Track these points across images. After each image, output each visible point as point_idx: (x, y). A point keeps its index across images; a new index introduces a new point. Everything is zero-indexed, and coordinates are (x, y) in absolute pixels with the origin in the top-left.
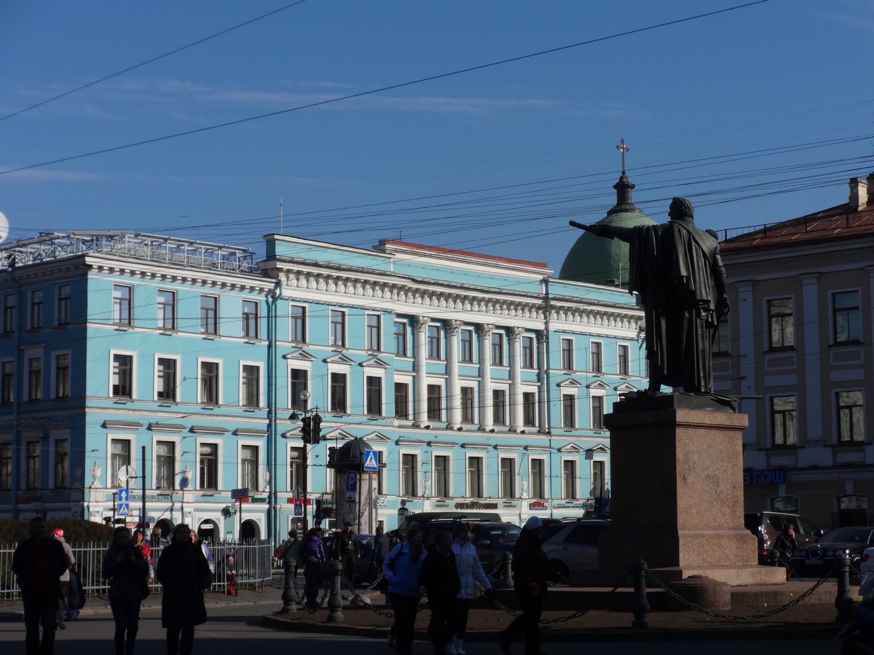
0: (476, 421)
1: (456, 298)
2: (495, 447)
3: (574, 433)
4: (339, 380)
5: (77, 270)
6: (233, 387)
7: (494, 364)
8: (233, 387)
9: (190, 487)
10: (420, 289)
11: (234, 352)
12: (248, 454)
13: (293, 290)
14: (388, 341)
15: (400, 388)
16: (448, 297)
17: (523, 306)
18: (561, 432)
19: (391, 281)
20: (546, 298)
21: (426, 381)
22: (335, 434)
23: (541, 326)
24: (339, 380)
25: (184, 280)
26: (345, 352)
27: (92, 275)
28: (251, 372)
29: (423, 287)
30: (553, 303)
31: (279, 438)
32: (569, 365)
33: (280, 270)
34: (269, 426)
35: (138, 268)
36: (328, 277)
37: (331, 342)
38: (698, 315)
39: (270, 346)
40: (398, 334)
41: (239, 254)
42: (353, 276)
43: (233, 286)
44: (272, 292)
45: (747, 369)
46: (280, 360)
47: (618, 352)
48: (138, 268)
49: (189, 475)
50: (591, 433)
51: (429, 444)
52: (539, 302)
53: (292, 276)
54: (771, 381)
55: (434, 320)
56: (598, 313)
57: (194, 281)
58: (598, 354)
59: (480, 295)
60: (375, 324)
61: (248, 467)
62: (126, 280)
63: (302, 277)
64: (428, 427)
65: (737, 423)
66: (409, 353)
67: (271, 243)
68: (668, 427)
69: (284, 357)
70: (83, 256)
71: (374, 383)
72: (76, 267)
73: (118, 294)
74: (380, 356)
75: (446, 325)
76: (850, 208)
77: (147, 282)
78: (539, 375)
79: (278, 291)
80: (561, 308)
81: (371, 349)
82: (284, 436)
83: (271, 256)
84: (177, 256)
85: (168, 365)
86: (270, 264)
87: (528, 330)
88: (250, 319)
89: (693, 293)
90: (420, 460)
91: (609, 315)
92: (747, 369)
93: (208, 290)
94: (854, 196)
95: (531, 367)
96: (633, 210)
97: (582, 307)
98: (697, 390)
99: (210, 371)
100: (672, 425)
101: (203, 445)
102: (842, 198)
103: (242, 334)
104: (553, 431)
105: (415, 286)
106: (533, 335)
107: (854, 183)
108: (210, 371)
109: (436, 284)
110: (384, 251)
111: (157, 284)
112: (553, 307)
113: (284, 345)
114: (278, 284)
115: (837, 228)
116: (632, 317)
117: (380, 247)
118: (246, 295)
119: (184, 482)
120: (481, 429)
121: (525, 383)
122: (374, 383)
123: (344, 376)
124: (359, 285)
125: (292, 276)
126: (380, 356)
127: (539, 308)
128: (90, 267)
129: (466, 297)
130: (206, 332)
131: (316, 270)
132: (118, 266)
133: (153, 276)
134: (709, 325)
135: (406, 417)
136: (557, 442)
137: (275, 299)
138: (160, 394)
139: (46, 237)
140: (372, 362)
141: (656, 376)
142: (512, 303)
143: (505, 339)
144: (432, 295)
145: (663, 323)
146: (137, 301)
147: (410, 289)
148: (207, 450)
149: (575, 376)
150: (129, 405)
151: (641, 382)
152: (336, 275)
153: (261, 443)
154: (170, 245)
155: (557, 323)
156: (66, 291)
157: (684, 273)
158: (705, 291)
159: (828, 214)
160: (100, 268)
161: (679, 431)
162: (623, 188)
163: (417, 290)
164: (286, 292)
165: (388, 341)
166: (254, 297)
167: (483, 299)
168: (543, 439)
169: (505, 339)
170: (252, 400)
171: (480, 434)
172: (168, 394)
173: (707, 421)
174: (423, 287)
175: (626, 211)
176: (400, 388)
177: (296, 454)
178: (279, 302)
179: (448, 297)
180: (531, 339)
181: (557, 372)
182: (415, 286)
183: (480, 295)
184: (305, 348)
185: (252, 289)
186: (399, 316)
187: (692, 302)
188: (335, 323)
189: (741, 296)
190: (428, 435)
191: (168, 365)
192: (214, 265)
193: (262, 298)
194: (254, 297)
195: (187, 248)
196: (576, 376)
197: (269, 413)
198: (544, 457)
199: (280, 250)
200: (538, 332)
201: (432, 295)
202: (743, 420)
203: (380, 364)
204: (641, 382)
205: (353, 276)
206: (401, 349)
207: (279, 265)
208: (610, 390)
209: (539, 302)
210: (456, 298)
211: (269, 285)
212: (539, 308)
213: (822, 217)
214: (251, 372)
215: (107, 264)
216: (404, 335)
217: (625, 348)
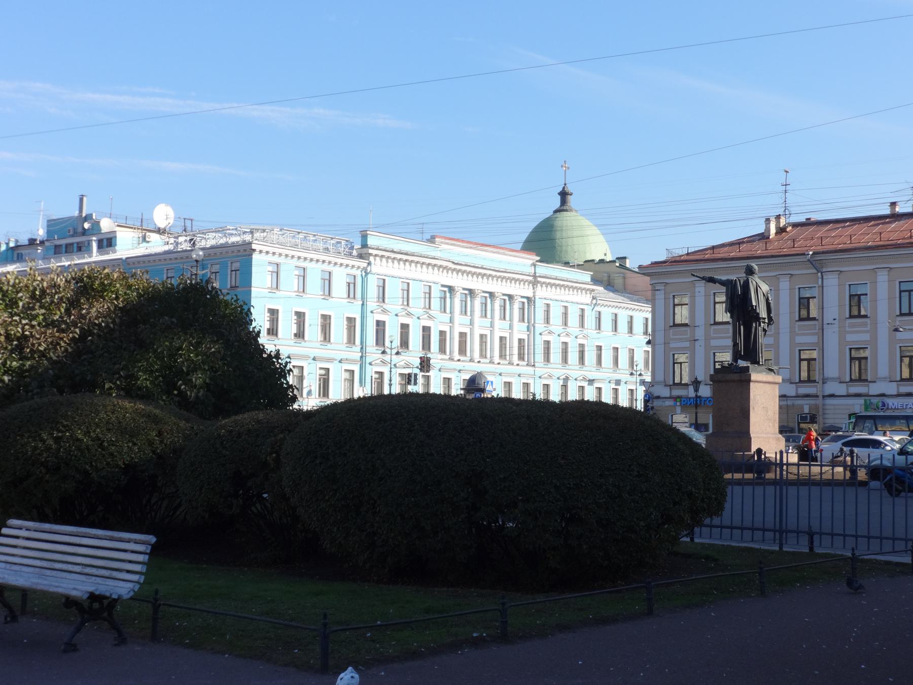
0: (488, 356)
1: (478, 275)
2: (500, 374)
3: (549, 366)
4: (405, 328)
5: (245, 252)
6: (338, 330)
7: (500, 319)
8: (338, 330)
9: (313, 396)
10: (457, 268)
11: (341, 309)
12: (347, 375)
13: (379, 267)
14: (436, 303)
15: (442, 333)
16: (473, 274)
17: (520, 281)
18: (542, 365)
19: (439, 263)
20: (535, 276)
21: (458, 330)
22: (402, 363)
23: (530, 295)
24: (405, 328)
25: (311, 260)
26: (409, 309)
27: (255, 256)
28: (351, 321)
29: (458, 267)
30: (539, 279)
31: (367, 365)
32: (547, 320)
33: (371, 254)
34: (362, 357)
35: (284, 252)
36: (382, 256)
37: (423, 306)
38: (760, 325)
39: (363, 304)
40: (379, 286)
41: (343, 243)
42: (416, 259)
43: (341, 265)
44: (365, 269)
45: (700, 333)
46: (369, 314)
47: (579, 313)
48: (284, 252)
49: (313, 388)
50: (560, 366)
51: (459, 371)
52: (531, 278)
53: (378, 258)
54: (714, 343)
55: (464, 289)
56: (567, 286)
57: (318, 261)
58: (565, 314)
59: (494, 273)
60: (381, 284)
61: (347, 384)
62: (276, 259)
63: (396, 262)
64: (459, 360)
65: (777, 381)
66: (469, 313)
67: (364, 237)
68: (745, 381)
69: (372, 312)
70: (250, 243)
71: (426, 330)
72: (245, 250)
73: (270, 268)
74: (431, 312)
75: (471, 292)
76: (763, 237)
77: (289, 260)
78: (528, 327)
79: (369, 269)
80: (544, 283)
81: (425, 308)
82: (370, 364)
83: (365, 245)
84: (309, 244)
85: (300, 316)
86: (364, 251)
87: (522, 297)
88: (351, 286)
89: (758, 314)
90: (453, 382)
91: (574, 288)
92: (700, 333)
93: (326, 267)
94: (768, 229)
95: (523, 321)
96: (571, 210)
97: (557, 282)
98: (758, 363)
99: (326, 319)
100: (749, 381)
101: (321, 368)
102: (761, 229)
103: (346, 296)
104: (536, 365)
105: (453, 266)
106: (506, 298)
107: (768, 221)
108: (326, 319)
109: (466, 265)
110: (434, 242)
111: (295, 262)
112: (538, 282)
113: (372, 304)
114: (369, 264)
115: (758, 249)
116: (588, 290)
117: (432, 240)
118: (349, 271)
119: (309, 393)
120: (492, 362)
121: (520, 331)
122: (426, 330)
123: (429, 328)
124: (390, 261)
125: (378, 258)
126: (431, 312)
127: (530, 282)
128: (254, 250)
129: (485, 275)
130: (324, 295)
131: (393, 255)
132: (271, 250)
133: (347, 266)
134: (764, 330)
135: (523, 360)
136: (539, 372)
137: (367, 274)
138: (295, 335)
139: (221, 230)
140: (425, 316)
141: (736, 356)
142: (513, 279)
143: (508, 302)
144: (463, 272)
145: (742, 328)
146: (282, 275)
147: (450, 269)
148: (323, 372)
149: (551, 328)
150: (303, 344)
151: (726, 357)
152: (405, 258)
153: (356, 368)
154: (301, 236)
155: (542, 293)
156: (236, 265)
157: (754, 304)
158: (763, 314)
159: (751, 240)
160: (261, 252)
161: (751, 384)
162: (564, 195)
163: (454, 269)
164: (374, 271)
165: (436, 303)
166: (354, 272)
167: (496, 276)
168: (530, 370)
169: (508, 302)
170: (351, 340)
171: (491, 365)
172: (300, 335)
173: (764, 380)
174: (458, 267)
175: (566, 211)
176: (442, 333)
177: (377, 376)
178: (369, 276)
179: (473, 274)
180: (523, 303)
181: (540, 327)
182: (453, 266)
183: (494, 273)
184: (385, 306)
185: (353, 267)
186: (443, 286)
187: (757, 318)
188: (403, 290)
189: (697, 290)
190: (459, 365)
191: (300, 316)
192: (296, 245)
193: (358, 273)
194: (354, 272)
195: (312, 238)
196: (551, 328)
197: (362, 348)
198: (531, 381)
199: (371, 241)
200: (528, 298)
201: (463, 272)
202: (779, 379)
203: (431, 317)
204: (726, 357)
205: (416, 259)
206: (381, 296)
207: (371, 251)
208: (573, 337)
209: (531, 278)
210: (478, 275)
211: (363, 264)
212: (530, 282)
213: (748, 242)
214: (351, 321)
215: (265, 249)
216: (445, 298)
217: (583, 310)
